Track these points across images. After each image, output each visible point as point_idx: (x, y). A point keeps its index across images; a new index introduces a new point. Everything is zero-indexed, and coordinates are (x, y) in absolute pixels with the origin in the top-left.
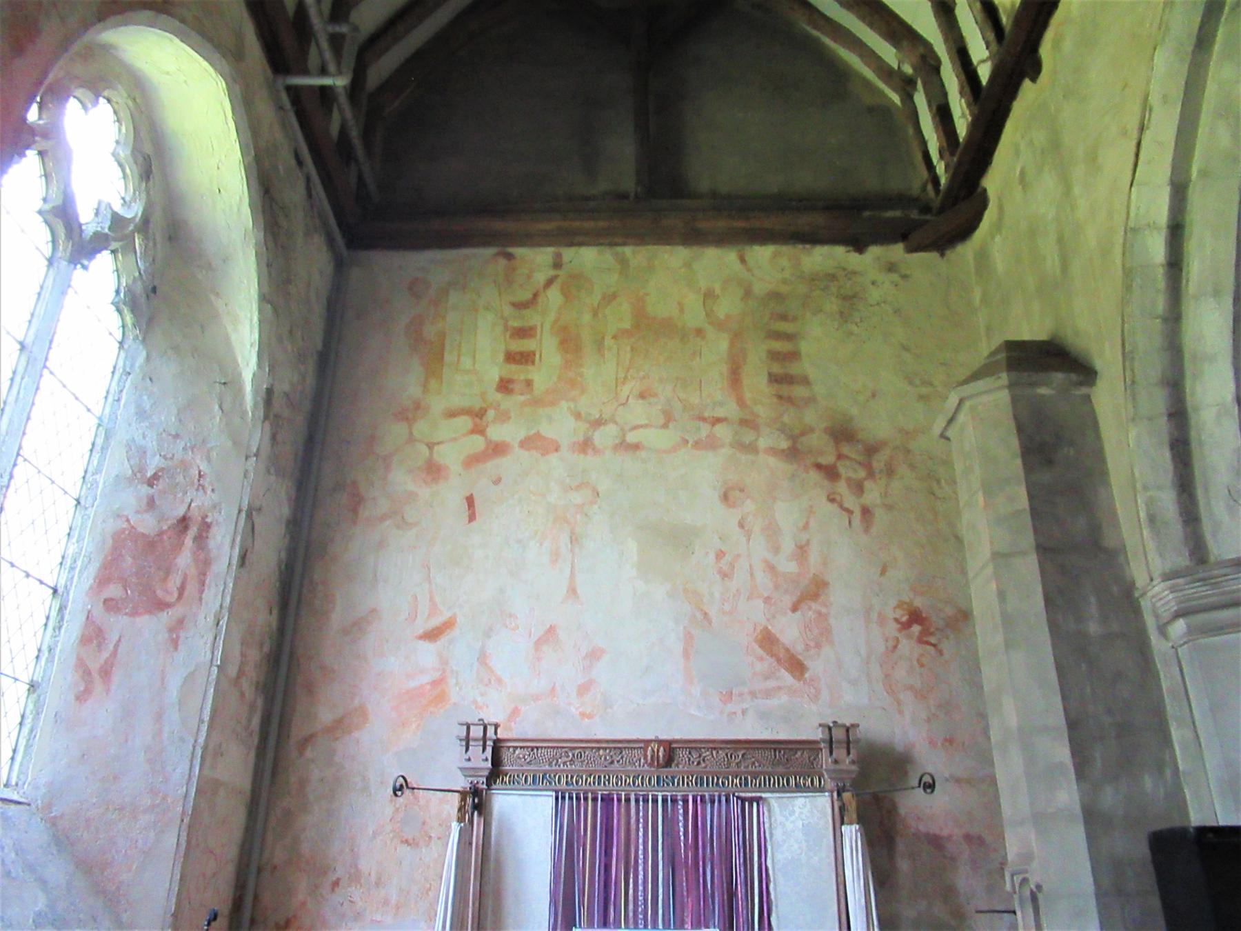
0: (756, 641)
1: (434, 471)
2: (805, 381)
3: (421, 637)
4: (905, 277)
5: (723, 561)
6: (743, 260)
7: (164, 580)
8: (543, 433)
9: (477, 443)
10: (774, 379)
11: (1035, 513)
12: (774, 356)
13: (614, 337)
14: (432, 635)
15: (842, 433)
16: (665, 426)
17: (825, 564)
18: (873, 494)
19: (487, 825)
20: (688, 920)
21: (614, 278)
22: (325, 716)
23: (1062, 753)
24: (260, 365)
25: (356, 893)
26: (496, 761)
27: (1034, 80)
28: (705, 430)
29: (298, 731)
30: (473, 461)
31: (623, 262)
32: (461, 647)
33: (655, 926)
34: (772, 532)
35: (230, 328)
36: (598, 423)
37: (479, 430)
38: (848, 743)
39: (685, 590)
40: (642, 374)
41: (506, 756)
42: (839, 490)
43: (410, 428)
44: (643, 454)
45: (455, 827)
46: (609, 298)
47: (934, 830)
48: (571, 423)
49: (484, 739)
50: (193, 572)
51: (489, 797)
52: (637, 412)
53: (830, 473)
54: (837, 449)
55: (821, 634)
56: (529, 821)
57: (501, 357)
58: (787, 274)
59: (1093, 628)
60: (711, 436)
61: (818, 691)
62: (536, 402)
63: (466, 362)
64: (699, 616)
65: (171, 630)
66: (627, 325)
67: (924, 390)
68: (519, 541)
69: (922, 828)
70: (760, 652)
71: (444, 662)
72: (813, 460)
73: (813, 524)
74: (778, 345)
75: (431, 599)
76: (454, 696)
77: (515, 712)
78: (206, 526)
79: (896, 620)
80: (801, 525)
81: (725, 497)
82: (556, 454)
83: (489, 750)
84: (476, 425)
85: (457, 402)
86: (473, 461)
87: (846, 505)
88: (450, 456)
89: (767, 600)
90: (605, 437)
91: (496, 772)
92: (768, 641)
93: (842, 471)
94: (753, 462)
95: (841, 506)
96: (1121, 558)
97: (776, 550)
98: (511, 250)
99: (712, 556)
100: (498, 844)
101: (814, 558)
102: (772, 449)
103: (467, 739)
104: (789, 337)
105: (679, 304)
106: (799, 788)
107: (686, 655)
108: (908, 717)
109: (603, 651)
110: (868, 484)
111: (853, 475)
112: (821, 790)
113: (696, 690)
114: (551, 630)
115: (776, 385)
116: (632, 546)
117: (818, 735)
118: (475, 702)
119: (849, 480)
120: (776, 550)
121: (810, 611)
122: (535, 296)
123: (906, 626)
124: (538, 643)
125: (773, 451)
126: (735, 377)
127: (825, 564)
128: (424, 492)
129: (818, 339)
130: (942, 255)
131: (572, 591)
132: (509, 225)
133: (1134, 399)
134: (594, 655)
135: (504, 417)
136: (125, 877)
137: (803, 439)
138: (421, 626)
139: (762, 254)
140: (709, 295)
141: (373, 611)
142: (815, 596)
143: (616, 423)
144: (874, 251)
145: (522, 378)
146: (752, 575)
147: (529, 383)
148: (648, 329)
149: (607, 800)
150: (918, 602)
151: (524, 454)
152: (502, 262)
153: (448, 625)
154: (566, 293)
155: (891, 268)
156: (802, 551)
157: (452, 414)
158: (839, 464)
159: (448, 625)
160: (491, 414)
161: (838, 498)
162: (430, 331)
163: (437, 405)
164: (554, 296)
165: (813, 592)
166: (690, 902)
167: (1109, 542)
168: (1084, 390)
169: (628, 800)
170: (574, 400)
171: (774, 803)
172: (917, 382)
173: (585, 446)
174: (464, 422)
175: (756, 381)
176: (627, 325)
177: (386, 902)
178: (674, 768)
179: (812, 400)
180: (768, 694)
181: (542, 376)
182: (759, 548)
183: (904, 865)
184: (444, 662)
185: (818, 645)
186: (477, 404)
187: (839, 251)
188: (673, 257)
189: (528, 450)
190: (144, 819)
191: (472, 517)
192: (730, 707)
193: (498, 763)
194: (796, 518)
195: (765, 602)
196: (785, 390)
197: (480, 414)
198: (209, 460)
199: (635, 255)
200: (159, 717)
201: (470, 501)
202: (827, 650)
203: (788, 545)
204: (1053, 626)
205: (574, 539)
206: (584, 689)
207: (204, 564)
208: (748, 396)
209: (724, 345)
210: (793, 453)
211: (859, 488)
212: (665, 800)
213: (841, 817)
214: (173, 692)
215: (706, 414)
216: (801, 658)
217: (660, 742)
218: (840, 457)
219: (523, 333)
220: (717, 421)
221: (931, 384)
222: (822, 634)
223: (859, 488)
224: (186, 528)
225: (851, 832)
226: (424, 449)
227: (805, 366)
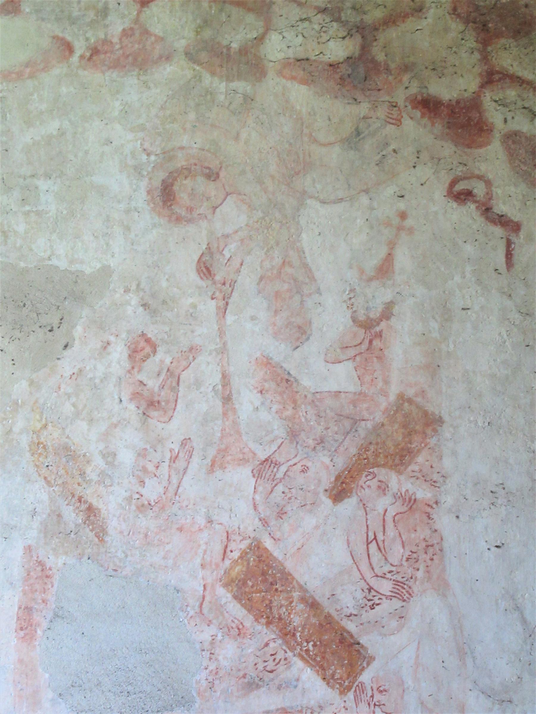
5: (152, 364)
17: (432, 368)
34: (291, 288)
39: (38, 447)
42: (483, 168)
53: (463, 122)
54: (485, 58)
55: (412, 559)
64: (71, 516)
70: (236, 611)
72: (414, 89)
73: (403, 259)
80: (372, 263)
81: (166, 195)
87: (501, 207)
92: (259, 580)
93: (495, 116)
94: (248, 99)
95: (486, 210)
97: (300, 333)
99: (119, 352)
101: (402, 346)
102: (302, 61)
107: (26, 625)
119: (512, 138)
121: (382, 496)
125: (302, 67)
127: (432, 368)
133: (254, 504)
137: (392, 33)
142: (400, 458)
146: (227, 399)
156: (370, 333)
158: (487, 99)
161: (479, 189)
182: (252, 332)
185: (402, 591)
195: (258, 474)
202: (426, 604)
203: (332, 319)
216: (351, 626)
218: (492, 77)
222: (414, 561)
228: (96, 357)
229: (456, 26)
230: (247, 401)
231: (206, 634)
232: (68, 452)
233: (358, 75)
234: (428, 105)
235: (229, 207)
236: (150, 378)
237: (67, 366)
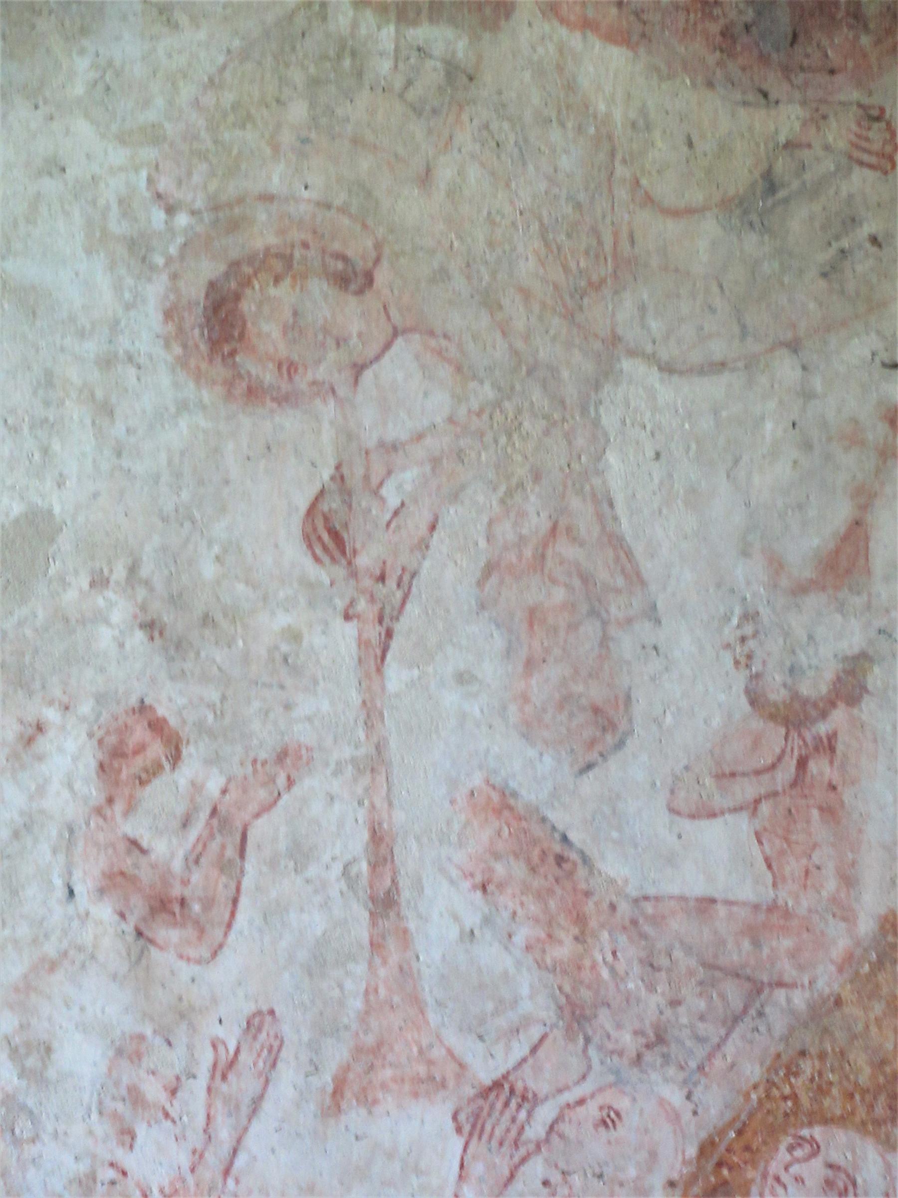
182: (459, 716)
203: (692, 695)
230: (442, 910)
235: (399, 367)
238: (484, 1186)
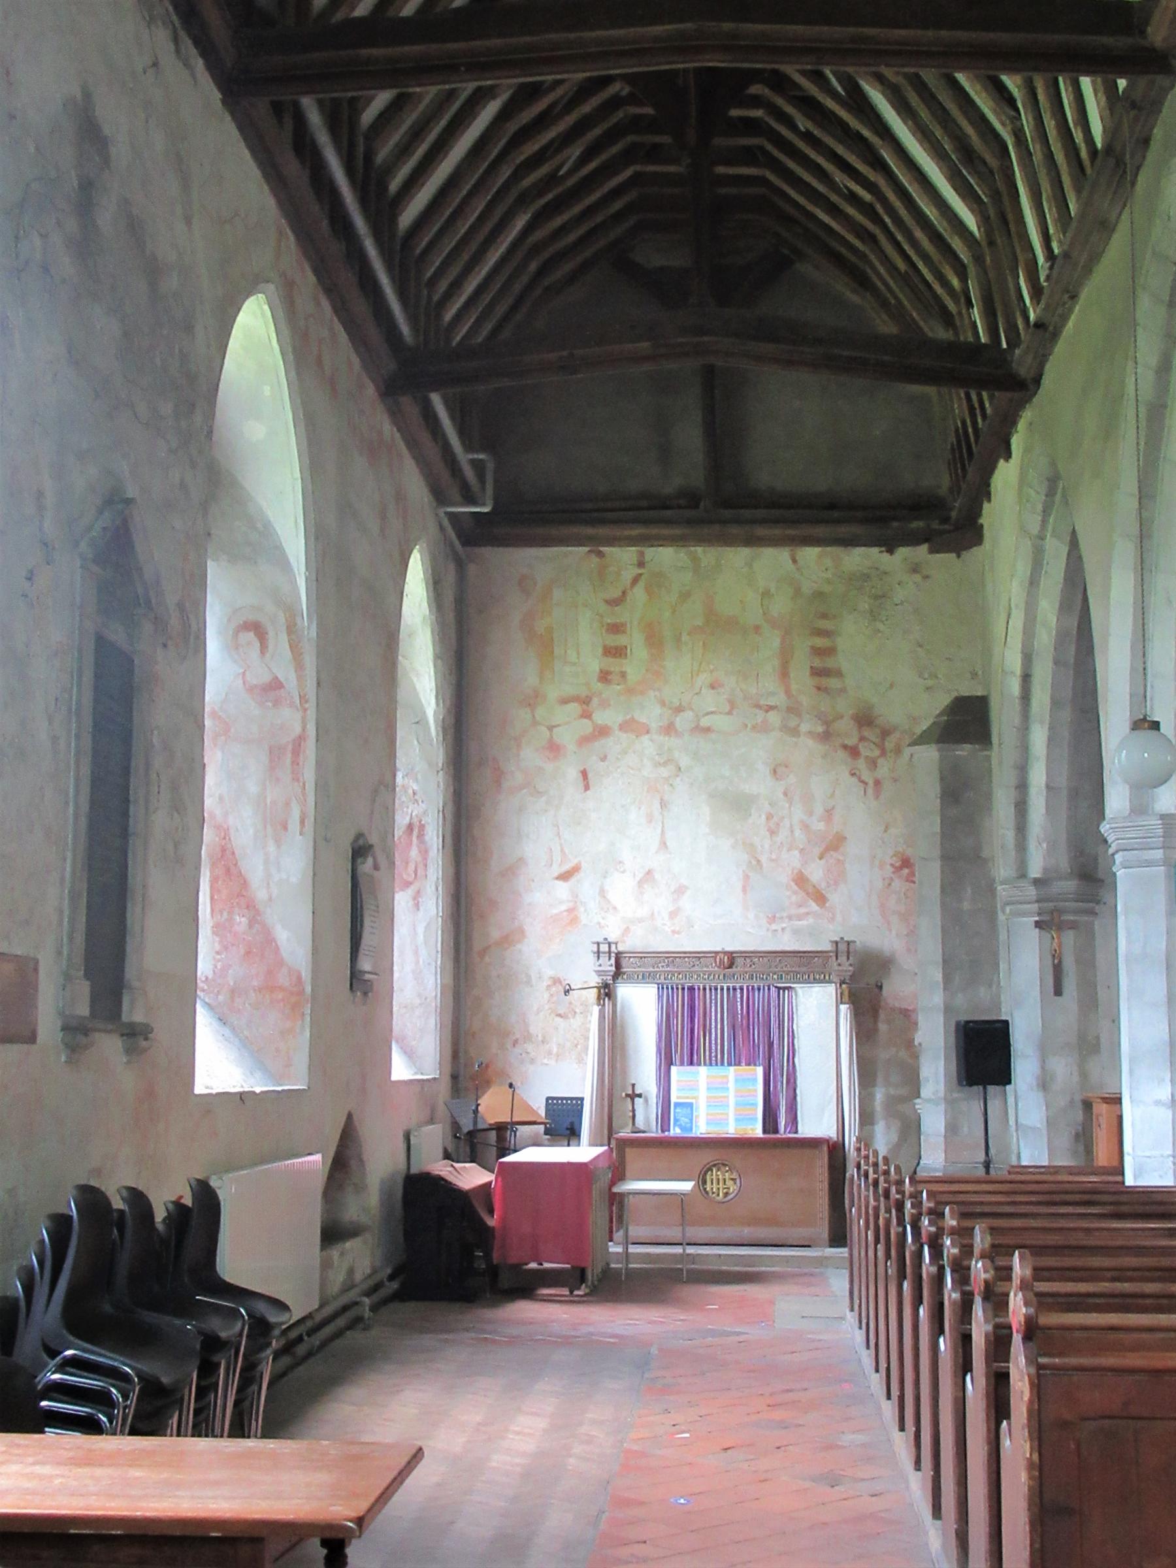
0: (793, 880)
1: (554, 749)
2: (839, 674)
3: (557, 878)
4: (926, 577)
6: (794, 561)
7: (406, 868)
8: (636, 717)
9: (586, 726)
10: (817, 672)
11: (943, 835)
12: (818, 652)
13: (689, 634)
14: (565, 877)
15: (865, 719)
16: (730, 713)
18: (884, 769)
19: (614, 1005)
20: (743, 1061)
21: (688, 576)
22: (495, 934)
23: (938, 976)
24: (437, 704)
25: (530, 1047)
26: (618, 965)
27: (989, 500)
28: (760, 716)
29: (477, 945)
30: (585, 740)
31: (695, 559)
32: (586, 885)
33: (722, 1064)
35: (415, 680)
36: (679, 710)
37: (587, 715)
38: (848, 952)
40: (712, 667)
41: (624, 962)
43: (533, 712)
44: (713, 736)
45: (596, 1009)
46: (685, 596)
47: (904, 1006)
48: (658, 710)
49: (610, 952)
50: (419, 859)
51: (615, 988)
52: (709, 700)
53: (854, 752)
56: (641, 1004)
57: (600, 650)
58: (829, 575)
59: (966, 905)
60: (765, 721)
61: (834, 915)
62: (630, 691)
63: (572, 655)
64: (754, 863)
65: (414, 899)
66: (699, 622)
67: (930, 683)
68: (623, 806)
69: (897, 1005)
70: (795, 887)
71: (575, 896)
74: (820, 642)
75: (562, 850)
76: (584, 919)
77: (627, 931)
78: (422, 827)
79: (892, 865)
82: (647, 737)
83: (613, 960)
84: (584, 711)
85: (569, 690)
86: (585, 740)
87: (863, 778)
88: (567, 736)
89: (802, 851)
90: (683, 721)
91: (618, 973)
92: (801, 880)
96: (990, 864)
98: (601, 549)
99: (764, 817)
100: (622, 1017)
103: (598, 952)
104: (826, 634)
105: (741, 601)
106: (816, 981)
107: (744, 890)
108: (894, 932)
109: (687, 888)
110: (880, 761)
111: (869, 754)
112: (830, 982)
113: (751, 915)
114: (649, 872)
115: (817, 679)
116: (706, 810)
117: (827, 947)
118: (599, 923)
119: (867, 757)
120: (810, 813)
122: (624, 593)
123: (898, 869)
124: (641, 883)
125: (810, 733)
126: (784, 674)
128: (549, 767)
129: (852, 634)
130: (959, 556)
131: (664, 844)
132: (602, 531)
134: (680, 891)
135: (605, 704)
136: (414, 1043)
138: (557, 870)
139: (810, 554)
140: (766, 594)
141: (521, 859)
143: (692, 709)
144: (903, 552)
145: (617, 669)
147: (623, 675)
148: (718, 627)
149: (691, 989)
150: (909, 852)
151: (624, 736)
152: (595, 560)
153: (576, 869)
154: (648, 590)
155: (915, 569)
156: (829, 813)
157: (565, 701)
159: (576, 869)
160: (595, 701)
162: (541, 626)
163: (553, 693)
164: (639, 594)
165: (835, 844)
166: (744, 1052)
167: (985, 854)
168: (986, 753)
169: (704, 989)
170: (659, 690)
171: (800, 991)
172: (926, 676)
173: (669, 729)
174: (574, 708)
175: (801, 678)
176: (699, 622)
177: (550, 1053)
178: (734, 969)
179: (843, 690)
180: (800, 918)
181: (634, 667)
182: (798, 813)
183: (883, 1027)
184: (575, 896)
185: (836, 883)
186: (583, 692)
187: (875, 551)
188: (737, 557)
189: (626, 732)
190: (417, 1013)
191: (587, 788)
192: (774, 927)
193: (619, 967)
194: (827, 788)
196: (825, 682)
197: (586, 701)
198: (416, 780)
199: (707, 555)
200: (416, 952)
201: (584, 774)
203: (819, 810)
204: (943, 905)
205: (663, 804)
206: (673, 915)
207: (424, 853)
208: (794, 687)
209: (776, 643)
210: (826, 736)
211: (873, 764)
212: (728, 989)
213: (840, 1000)
214: (421, 938)
215: (762, 702)
217: (725, 953)
218: (862, 739)
219: (616, 629)
220: (770, 708)
221: (937, 677)
222: (838, 876)
223: (873, 764)
224: (412, 830)
225: (844, 1008)
226: (544, 729)
227: (842, 661)
228: (758, 819)
229: (852, 722)
230: (797, 833)
231: (788, 893)
232: (752, 845)
233: (826, 737)
234: (845, 747)
235: (791, 776)
236: (772, 824)
237: (750, 821)
238: (368, 116)
